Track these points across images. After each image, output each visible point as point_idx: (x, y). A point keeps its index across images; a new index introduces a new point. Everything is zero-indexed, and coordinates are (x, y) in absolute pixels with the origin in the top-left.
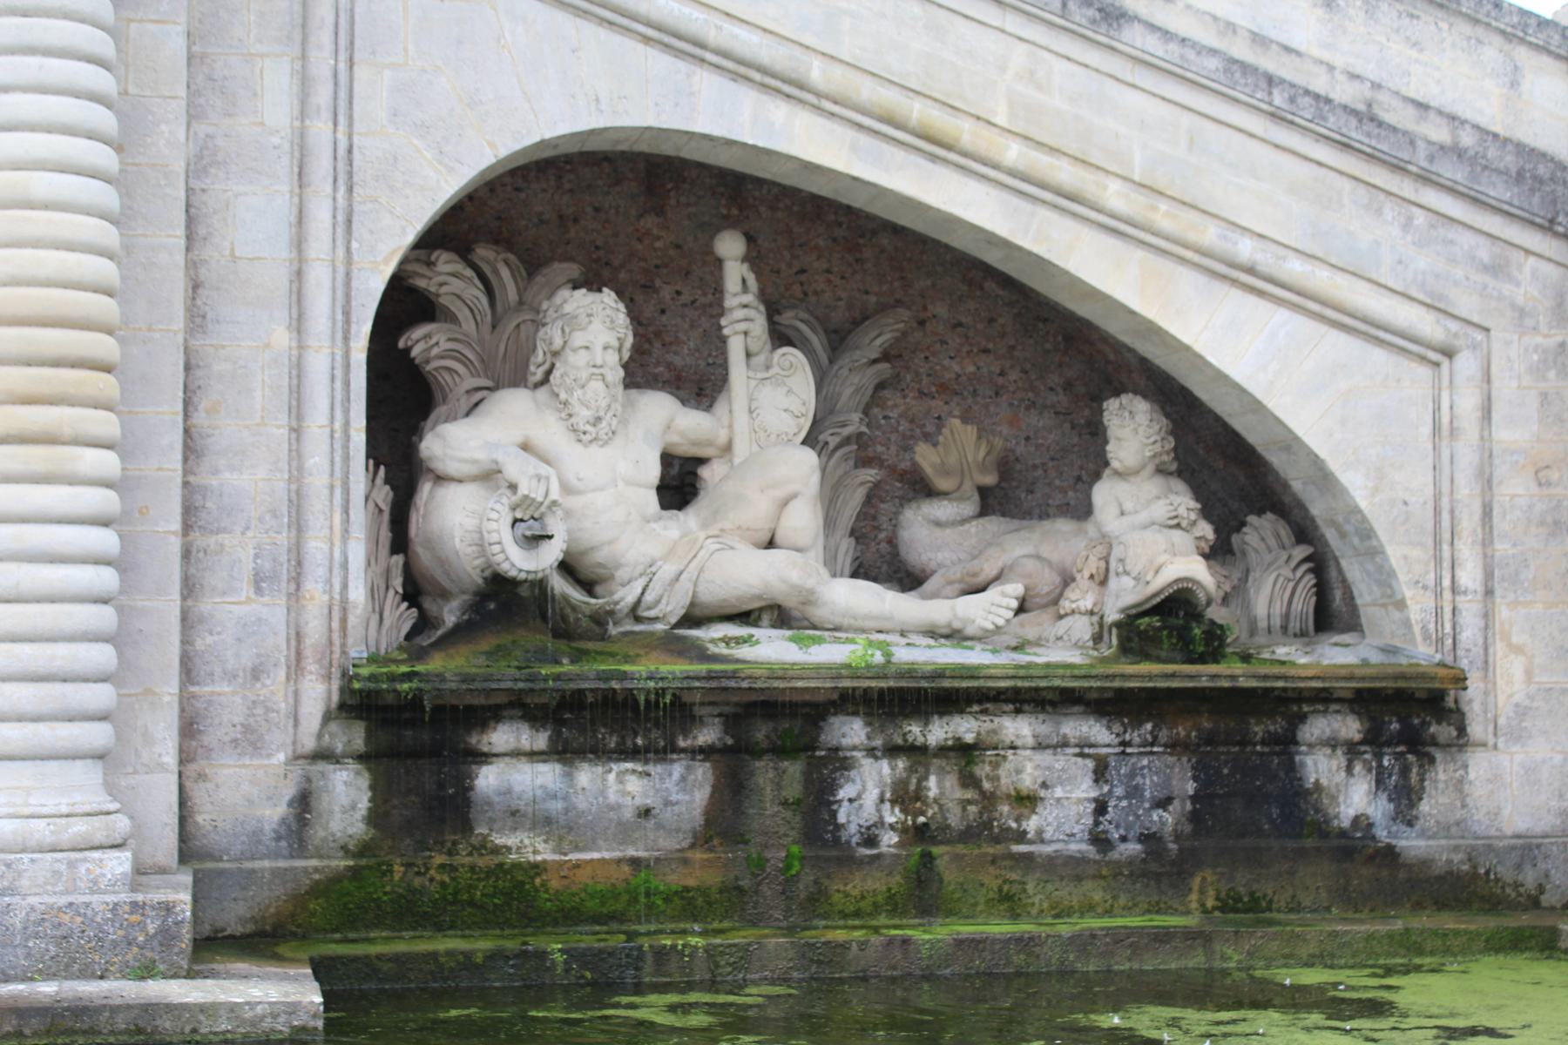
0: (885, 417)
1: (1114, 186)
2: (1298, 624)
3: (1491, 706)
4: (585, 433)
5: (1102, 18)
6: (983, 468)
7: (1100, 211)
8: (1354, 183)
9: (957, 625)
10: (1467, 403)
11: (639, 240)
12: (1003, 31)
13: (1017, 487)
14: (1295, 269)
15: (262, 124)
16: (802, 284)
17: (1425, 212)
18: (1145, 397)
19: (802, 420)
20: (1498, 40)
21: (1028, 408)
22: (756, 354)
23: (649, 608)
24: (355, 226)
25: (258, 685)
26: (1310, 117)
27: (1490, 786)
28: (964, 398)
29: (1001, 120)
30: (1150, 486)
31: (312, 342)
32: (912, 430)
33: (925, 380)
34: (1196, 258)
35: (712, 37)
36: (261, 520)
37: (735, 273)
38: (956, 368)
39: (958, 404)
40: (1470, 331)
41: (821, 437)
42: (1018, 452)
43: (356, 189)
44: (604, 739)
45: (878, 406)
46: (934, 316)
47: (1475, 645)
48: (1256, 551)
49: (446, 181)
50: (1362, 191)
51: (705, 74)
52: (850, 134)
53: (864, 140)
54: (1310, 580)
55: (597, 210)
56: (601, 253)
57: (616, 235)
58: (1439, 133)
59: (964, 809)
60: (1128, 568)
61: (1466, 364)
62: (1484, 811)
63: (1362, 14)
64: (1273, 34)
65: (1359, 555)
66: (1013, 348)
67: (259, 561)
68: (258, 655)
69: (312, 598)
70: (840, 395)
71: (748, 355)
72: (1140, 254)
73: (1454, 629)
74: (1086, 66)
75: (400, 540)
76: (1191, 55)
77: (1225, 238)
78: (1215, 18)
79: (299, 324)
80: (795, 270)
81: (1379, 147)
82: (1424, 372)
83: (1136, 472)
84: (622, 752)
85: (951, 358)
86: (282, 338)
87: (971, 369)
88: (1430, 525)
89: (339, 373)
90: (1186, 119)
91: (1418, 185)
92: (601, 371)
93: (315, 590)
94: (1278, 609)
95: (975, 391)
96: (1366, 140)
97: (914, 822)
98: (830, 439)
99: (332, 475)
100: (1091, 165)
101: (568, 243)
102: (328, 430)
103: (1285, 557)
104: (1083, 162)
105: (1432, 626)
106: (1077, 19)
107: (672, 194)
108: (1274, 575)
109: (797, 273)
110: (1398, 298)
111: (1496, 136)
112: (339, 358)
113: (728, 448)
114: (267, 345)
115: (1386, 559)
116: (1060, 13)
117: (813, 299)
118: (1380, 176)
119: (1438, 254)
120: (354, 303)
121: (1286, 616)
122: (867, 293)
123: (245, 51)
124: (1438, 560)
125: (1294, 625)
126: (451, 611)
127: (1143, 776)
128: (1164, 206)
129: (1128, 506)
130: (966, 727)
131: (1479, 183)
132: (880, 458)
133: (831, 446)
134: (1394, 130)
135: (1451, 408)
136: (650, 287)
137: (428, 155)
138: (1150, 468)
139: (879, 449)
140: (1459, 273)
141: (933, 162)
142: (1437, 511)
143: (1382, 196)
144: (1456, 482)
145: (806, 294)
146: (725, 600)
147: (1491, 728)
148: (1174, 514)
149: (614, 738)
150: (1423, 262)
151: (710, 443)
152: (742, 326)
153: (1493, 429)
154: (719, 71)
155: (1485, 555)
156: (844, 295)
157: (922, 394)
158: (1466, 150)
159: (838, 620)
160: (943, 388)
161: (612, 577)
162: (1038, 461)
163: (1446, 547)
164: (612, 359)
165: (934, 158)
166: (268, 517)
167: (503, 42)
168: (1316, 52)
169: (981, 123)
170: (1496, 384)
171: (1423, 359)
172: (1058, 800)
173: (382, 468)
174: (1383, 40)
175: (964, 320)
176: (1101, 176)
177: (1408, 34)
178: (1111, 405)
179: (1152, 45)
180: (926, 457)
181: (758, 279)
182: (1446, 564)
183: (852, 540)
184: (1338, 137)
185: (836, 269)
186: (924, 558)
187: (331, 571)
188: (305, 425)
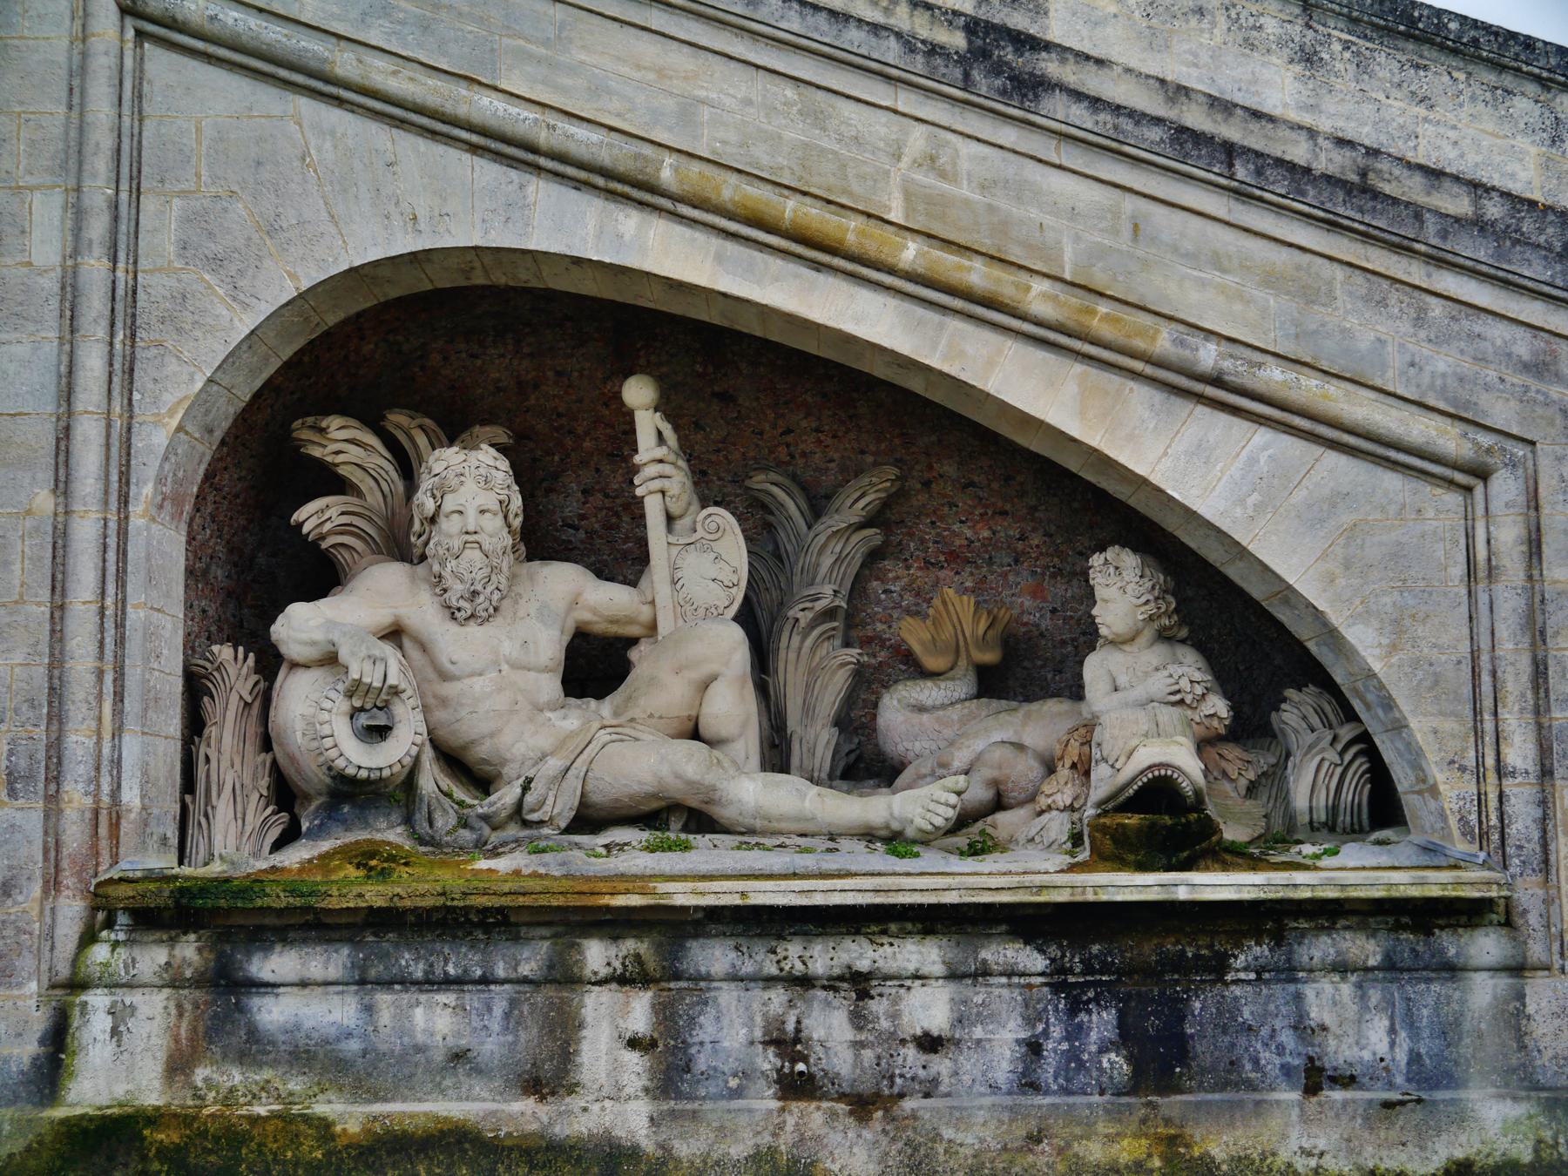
0: (885, 592)
1: (1039, 286)
2: (1348, 819)
3: (1555, 919)
4: (459, 609)
5: (1013, 88)
6: (983, 643)
7: (1024, 318)
8: (1349, 270)
9: (895, 826)
10: (1509, 534)
11: (606, 405)
12: (896, 112)
13: (1042, 667)
14: (1274, 377)
15: (30, 264)
16: (788, 446)
17: (1443, 302)
18: (1135, 550)
19: (734, 590)
20: (1532, 88)
21: (1053, 576)
22: (681, 517)
23: (533, 811)
24: (136, 375)
25: (9, 902)
26: (1283, 192)
27: (1557, 1022)
28: (977, 567)
29: (894, 216)
30: (1154, 655)
31: (77, 507)
32: (917, 604)
33: (932, 547)
34: (1149, 370)
35: (543, 138)
36: (16, 711)
37: (648, 424)
38: (969, 533)
39: (972, 574)
40: (1509, 445)
41: (791, 613)
42: (1043, 627)
43: (141, 334)
44: (408, 966)
45: (878, 579)
46: (941, 476)
47: (1529, 841)
48: (1296, 731)
49: (241, 320)
50: (1359, 278)
51: (542, 184)
52: (716, 242)
53: (731, 247)
54: (1361, 765)
55: (558, 374)
56: (564, 421)
57: (580, 401)
58: (1458, 204)
59: (857, 1056)
60: (1105, 754)
61: (1505, 488)
62: (1549, 1053)
63: (1352, 68)
64: (1239, 98)
65: (1387, 731)
66: (1034, 509)
67: (13, 759)
68: (10, 868)
69: (70, 801)
70: (818, 565)
71: (670, 519)
72: (1078, 368)
73: (1502, 820)
74: (1001, 147)
75: (266, 744)
76: (1127, 124)
77: (1182, 343)
78: (1162, 82)
79: (63, 486)
80: (780, 431)
81: (1374, 223)
82: (1453, 499)
83: (1131, 639)
84: (432, 983)
85: (962, 522)
86: (45, 501)
87: (986, 534)
88: (1467, 690)
89: (112, 541)
90: (1129, 204)
91: (1431, 269)
92: (475, 538)
93: (76, 796)
94: (1321, 800)
95: (990, 558)
96: (1358, 216)
97: (792, 1068)
98: (800, 615)
99: (101, 656)
100: (1012, 264)
101: (527, 411)
102: (94, 608)
103: (1330, 738)
104: (1001, 260)
105: (1473, 817)
106: (984, 91)
107: (642, 353)
108: (1318, 759)
109: (782, 434)
110: (1414, 408)
111: (1532, 204)
112: (113, 525)
113: (653, 627)
114: (29, 512)
115: (1411, 735)
116: (960, 85)
117: (800, 462)
118: (1379, 259)
119: (1462, 352)
120: (133, 462)
121: (1333, 810)
122: (863, 452)
123: (13, 184)
124: (1478, 734)
125: (1344, 819)
126: (307, 816)
127: (1089, 1012)
128: (1103, 308)
129: (1122, 680)
130: (860, 954)
131: (1509, 262)
132: (880, 638)
133: (803, 623)
134: (1395, 201)
135: (1488, 542)
136: (617, 456)
137: (221, 291)
138: (1148, 634)
139: (880, 627)
140: (1491, 375)
141: (818, 271)
142: (1475, 674)
143: (1385, 284)
144: (1497, 635)
145: (792, 456)
146: (617, 800)
147: (1556, 946)
148: (1176, 687)
149: (421, 966)
150: (1443, 363)
151: (630, 621)
152: (657, 484)
153: (1545, 566)
154: (558, 179)
155: (1539, 726)
156: (836, 456)
157: (928, 564)
158: (1493, 223)
159: (749, 821)
160: (953, 557)
161: (499, 775)
162: (1066, 636)
163: (1487, 717)
164: (494, 523)
165: (818, 266)
166: (25, 707)
167: (308, 160)
168: (1294, 116)
169: (873, 222)
170: (1546, 510)
171: (1451, 483)
172: (979, 1041)
173: (251, 655)
174: (1382, 97)
175: (976, 479)
176: (1023, 277)
177: (1413, 88)
178: (1096, 560)
179: (1079, 114)
180: (914, 634)
181: (676, 428)
182: (1489, 739)
183: (835, 731)
184: (1321, 214)
185: (827, 428)
186: (901, 748)
187: (98, 769)
188: (67, 601)
